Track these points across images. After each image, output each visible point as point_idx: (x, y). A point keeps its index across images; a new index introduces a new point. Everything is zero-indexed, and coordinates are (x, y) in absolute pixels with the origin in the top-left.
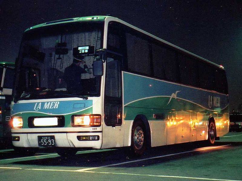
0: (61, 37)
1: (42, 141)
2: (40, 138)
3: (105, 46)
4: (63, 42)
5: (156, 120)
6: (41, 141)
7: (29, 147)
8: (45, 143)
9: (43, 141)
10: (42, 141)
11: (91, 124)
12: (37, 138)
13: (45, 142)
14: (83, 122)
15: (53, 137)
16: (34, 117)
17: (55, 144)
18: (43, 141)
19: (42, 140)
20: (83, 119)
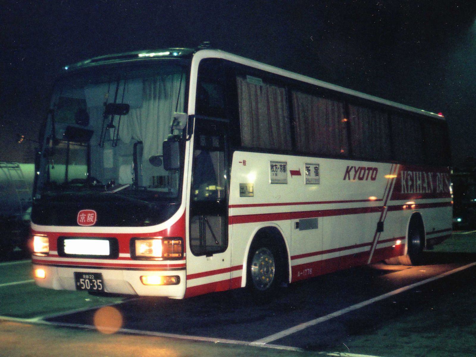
0: (115, 86)
1: (82, 281)
2: (78, 276)
3: (192, 110)
4: (119, 101)
5: (60, 257)
6: (79, 282)
7: (62, 289)
8: (100, 285)
9: (84, 282)
10: (82, 281)
11: (165, 255)
12: (72, 276)
13: (99, 284)
14: (150, 251)
15: (98, 276)
16: (135, 238)
17: (103, 288)
18: (84, 282)
19: (82, 280)
20: (150, 245)
